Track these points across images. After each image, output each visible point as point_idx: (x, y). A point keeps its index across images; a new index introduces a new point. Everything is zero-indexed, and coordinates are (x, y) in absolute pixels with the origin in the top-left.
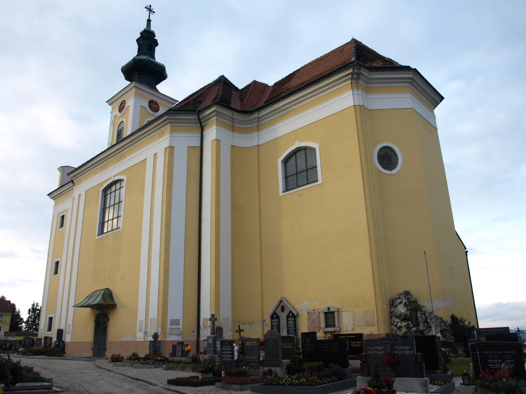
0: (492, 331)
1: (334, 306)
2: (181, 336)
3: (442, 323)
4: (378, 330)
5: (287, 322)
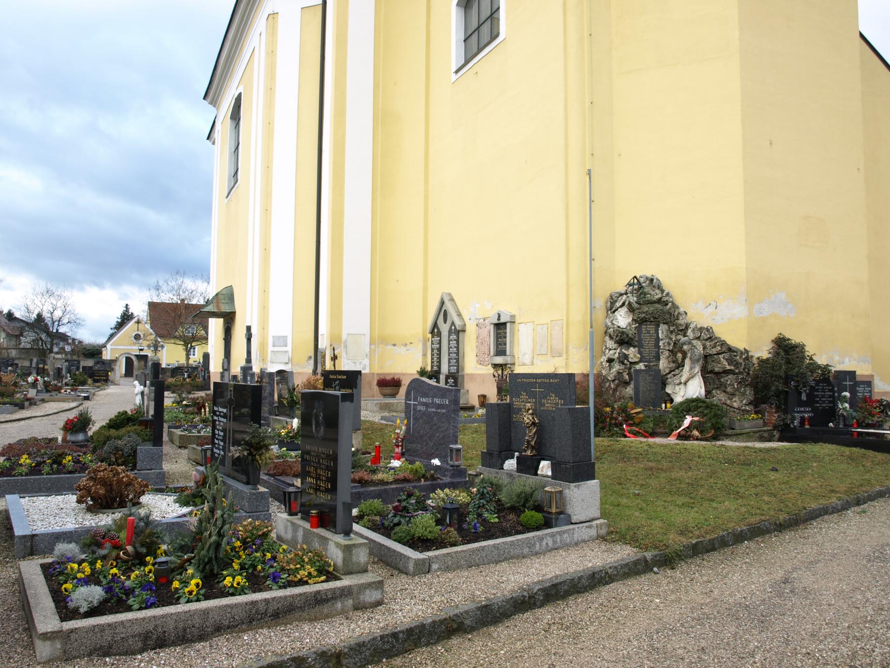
0: (536, 382)
1: (507, 310)
2: (290, 365)
3: (722, 355)
4: (567, 364)
5: (449, 344)
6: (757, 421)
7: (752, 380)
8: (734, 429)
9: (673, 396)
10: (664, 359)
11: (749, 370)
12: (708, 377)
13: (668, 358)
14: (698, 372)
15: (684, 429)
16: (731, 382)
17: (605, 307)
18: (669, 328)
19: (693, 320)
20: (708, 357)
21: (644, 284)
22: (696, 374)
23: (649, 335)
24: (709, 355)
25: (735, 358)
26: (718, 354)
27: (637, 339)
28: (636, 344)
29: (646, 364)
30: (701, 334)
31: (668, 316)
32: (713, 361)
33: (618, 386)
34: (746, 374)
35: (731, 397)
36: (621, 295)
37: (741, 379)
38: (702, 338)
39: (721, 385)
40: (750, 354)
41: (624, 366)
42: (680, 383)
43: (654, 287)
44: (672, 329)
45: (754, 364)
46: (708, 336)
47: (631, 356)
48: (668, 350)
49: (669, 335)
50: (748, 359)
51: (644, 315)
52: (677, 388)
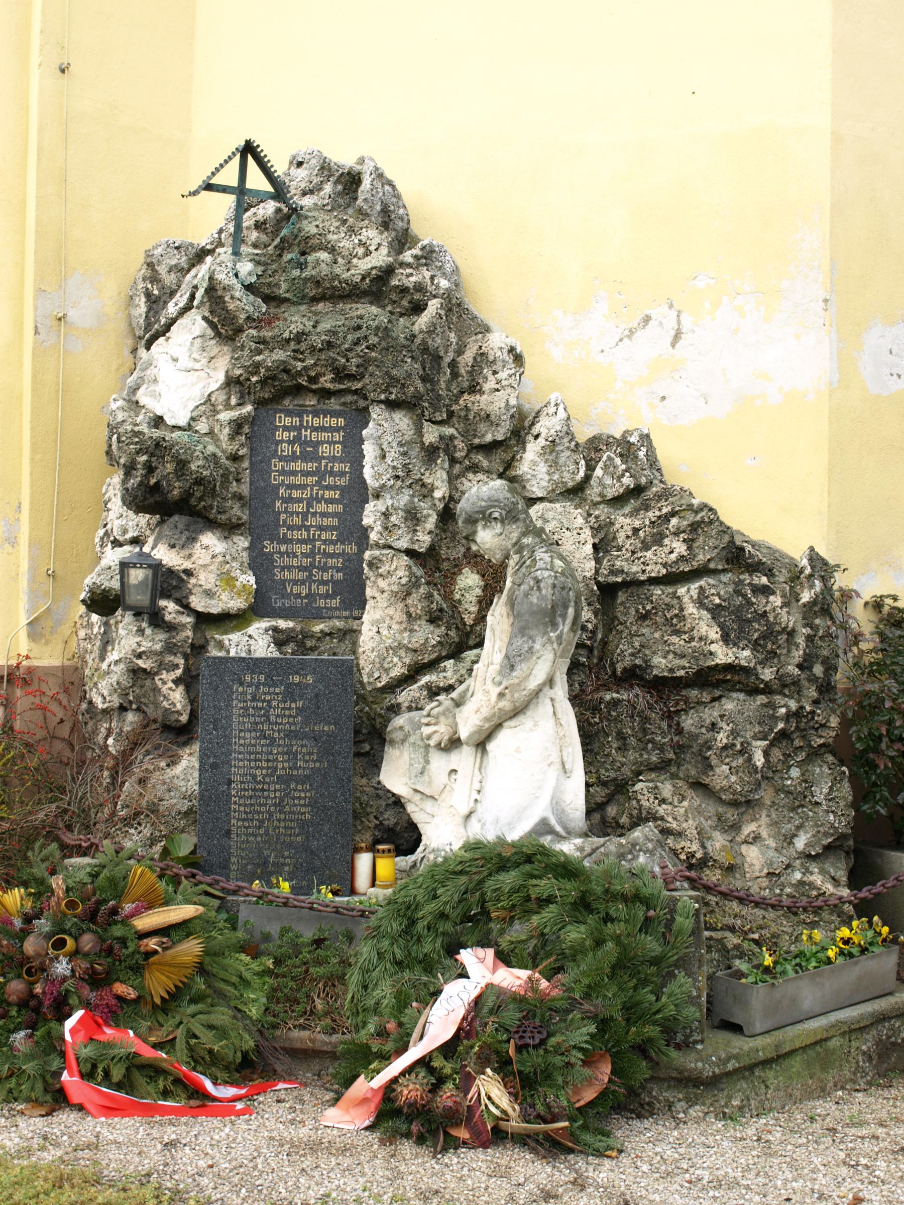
3: (694, 587)
6: (866, 964)
7: (845, 723)
8: (737, 1029)
9: (416, 812)
10: (383, 600)
11: (830, 668)
12: (615, 703)
13: (406, 593)
14: (550, 682)
15: (424, 1062)
16: (734, 733)
17: (123, 326)
18: (419, 432)
19: (553, 397)
20: (621, 597)
21: (307, 202)
22: (537, 693)
23: (311, 466)
24: (626, 585)
25: (759, 602)
26: (673, 578)
27: (245, 489)
28: (237, 511)
29: (283, 624)
30: (590, 468)
31: (411, 366)
32: (644, 617)
33: (134, 743)
34: (813, 693)
35: (731, 815)
36: (201, 255)
37: (788, 717)
38: (593, 492)
39: (680, 748)
40: (840, 581)
41: (162, 636)
42: (454, 743)
43: (362, 214)
44: (431, 435)
45: (857, 638)
46: (627, 481)
47: (206, 579)
48: (410, 553)
49: (418, 469)
50: (826, 612)
51: (280, 355)
52: (439, 763)
